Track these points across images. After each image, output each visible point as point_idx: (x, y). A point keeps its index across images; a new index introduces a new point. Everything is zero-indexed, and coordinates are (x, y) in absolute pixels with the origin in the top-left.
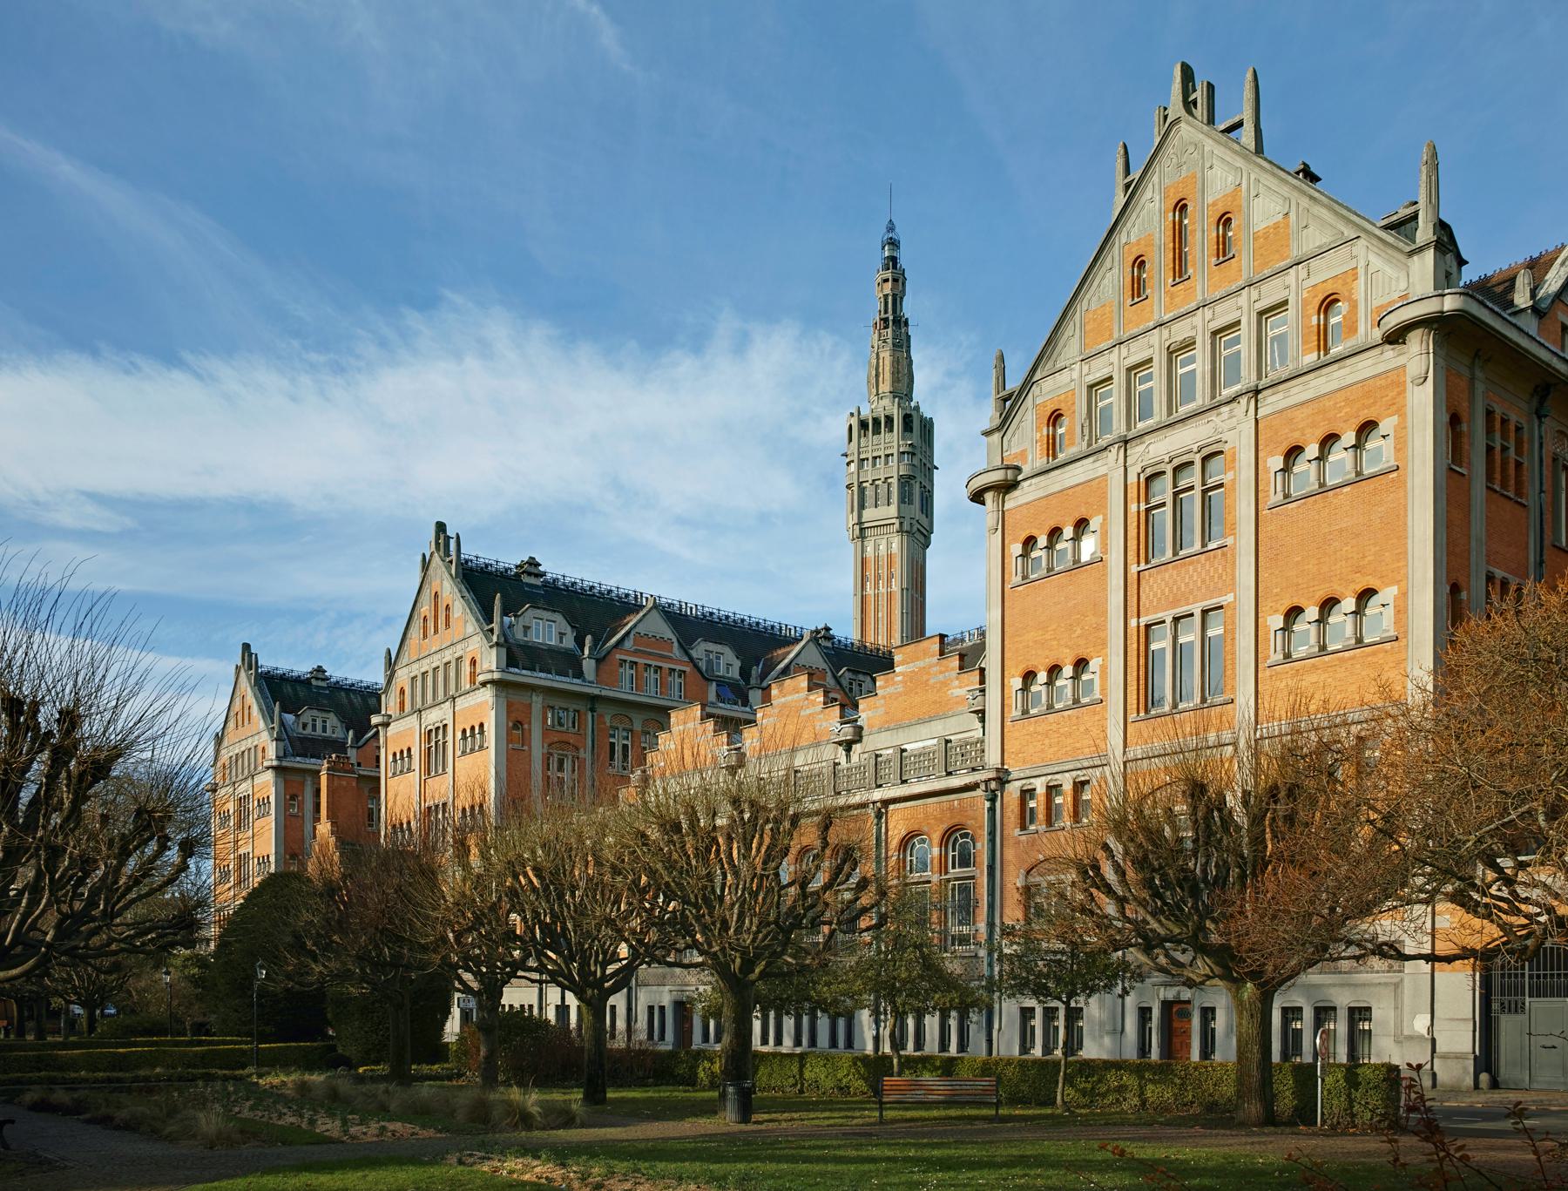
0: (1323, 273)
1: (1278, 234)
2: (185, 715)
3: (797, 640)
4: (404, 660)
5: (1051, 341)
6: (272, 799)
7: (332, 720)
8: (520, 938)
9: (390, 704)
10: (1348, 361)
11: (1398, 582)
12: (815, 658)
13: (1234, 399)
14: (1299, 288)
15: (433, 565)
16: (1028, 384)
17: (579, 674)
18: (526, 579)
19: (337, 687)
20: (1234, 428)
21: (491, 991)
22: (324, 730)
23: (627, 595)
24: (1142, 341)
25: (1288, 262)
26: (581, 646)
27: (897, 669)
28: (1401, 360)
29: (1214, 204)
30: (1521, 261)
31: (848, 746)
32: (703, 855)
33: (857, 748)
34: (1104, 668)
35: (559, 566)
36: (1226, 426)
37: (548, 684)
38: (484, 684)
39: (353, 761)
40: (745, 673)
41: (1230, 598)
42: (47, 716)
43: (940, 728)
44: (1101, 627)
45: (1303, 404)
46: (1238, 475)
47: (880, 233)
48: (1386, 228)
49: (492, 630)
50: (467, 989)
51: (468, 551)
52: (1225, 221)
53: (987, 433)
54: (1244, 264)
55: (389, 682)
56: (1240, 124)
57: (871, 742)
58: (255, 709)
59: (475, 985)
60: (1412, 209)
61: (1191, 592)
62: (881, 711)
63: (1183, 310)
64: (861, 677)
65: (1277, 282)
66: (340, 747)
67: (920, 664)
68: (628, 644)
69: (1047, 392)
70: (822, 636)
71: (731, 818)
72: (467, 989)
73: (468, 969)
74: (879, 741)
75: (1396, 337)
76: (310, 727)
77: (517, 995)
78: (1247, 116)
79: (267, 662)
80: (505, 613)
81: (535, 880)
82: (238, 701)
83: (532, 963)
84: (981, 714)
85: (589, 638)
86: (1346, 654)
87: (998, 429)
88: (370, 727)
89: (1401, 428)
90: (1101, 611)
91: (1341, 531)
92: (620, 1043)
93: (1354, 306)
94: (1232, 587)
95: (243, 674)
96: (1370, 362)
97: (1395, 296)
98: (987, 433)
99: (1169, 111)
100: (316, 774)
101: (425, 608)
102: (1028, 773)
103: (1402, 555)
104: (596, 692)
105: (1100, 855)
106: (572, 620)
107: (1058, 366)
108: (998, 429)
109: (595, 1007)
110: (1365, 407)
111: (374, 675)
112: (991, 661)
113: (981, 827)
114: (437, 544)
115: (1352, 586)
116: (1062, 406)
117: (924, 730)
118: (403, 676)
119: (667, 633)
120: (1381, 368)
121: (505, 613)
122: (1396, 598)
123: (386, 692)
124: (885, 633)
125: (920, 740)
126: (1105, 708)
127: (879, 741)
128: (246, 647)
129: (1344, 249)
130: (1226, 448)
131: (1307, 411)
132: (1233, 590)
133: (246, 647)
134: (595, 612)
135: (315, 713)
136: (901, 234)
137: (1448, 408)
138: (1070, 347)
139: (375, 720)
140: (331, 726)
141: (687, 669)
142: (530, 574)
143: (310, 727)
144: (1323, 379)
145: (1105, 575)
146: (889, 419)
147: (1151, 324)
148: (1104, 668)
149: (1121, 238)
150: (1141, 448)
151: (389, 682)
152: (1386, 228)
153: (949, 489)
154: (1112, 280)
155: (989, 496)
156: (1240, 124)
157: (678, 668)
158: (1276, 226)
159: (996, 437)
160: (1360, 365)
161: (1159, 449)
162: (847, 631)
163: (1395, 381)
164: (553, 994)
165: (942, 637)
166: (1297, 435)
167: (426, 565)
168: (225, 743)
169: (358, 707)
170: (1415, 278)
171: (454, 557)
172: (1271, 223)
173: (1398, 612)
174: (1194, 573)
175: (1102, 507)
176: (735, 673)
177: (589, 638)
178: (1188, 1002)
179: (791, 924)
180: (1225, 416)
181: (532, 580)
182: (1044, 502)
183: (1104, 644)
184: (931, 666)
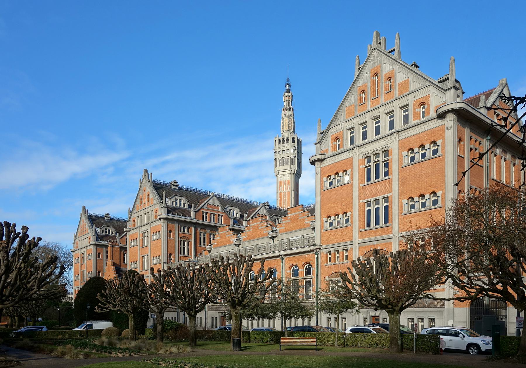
0: (420, 96)
1: (405, 85)
2: (59, 232)
3: (258, 206)
4: (135, 211)
5: (336, 116)
6: (93, 254)
7: (184, 201)
8: (169, 295)
9: (130, 224)
10: (427, 123)
11: (442, 190)
12: (263, 211)
13: (392, 134)
14: (411, 100)
15: (143, 182)
16: (329, 129)
17: (190, 216)
18: (173, 187)
19: (113, 219)
20: (393, 144)
21: (161, 312)
22: (109, 232)
23: (205, 192)
24: (363, 116)
25: (408, 93)
26: (116, 235)
27: (289, 215)
28: (351, 156)
29: (386, 75)
30: (482, 92)
31: (273, 238)
32: (225, 270)
33: (240, 246)
34: (352, 215)
35: (183, 181)
36: (390, 142)
37: (180, 219)
38: (160, 219)
39: (118, 242)
40: (242, 216)
41: (391, 194)
42: (18, 229)
43: (301, 233)
44: (351, 202)
45: (413, 136)
46: (394, 158)
47: (285, 81)
48: (439, 82)
49: (162, 202)
50: (154, 311)
51: (155, 178)
52: (390, 79)
53: (316, 144)
54: (396, 93)
55: (130, 218)
56: (394, 50)
57: (280, 237)
58: (87, 226)
59: (156, 311)
60: (447, 77)
61: (379, 192)
62: (284, 228)
63: (376, 107)
64: (278, 217)
65: (405, 99)
66: (114, 238)
67: (296, 213)
68: (205, 207)
69: (333, 132)
70: (266, 205)
71: (235, 260)
72: (154, 311)
73: (153, 305)
74: (284, 237)
75: (442, 116)
76: (174, 203)
77: (169, 315)
78: (396, 48)
79: (91, 212)
80: (166, 197)
81: (174, 278)
82: (81, 223)
83: (174, 303)
84: (314, 229)
85: (118, 234)
86: (427, 211)
87: (319, 143)
88: (124, 232)
89: (352, 172)
90: (351, 197)
91: (425, 174)
92: (202, 328)
93: (429, 106)
94: (391, 191)
95: (83, 215)
96: (434, 123)
97: (442, 103)
98: (316, 144)
99: (372, 46)
100: (106, 246)
101: (141, 195)
102: (329, 247)
103: (444, 181)
104: (195, 221)
105: (347, 271)
106: (188, 199)
107: (338, 124)
108: (319, 143)
109: (193, 317)
110: (432, 137)
111: (125, 216)
112: (318, 213)
113: (314, 263)
114: (145, 176)
115: (428, 191)
116: (339, 136)
117: (297, 234)
118: (134, 216)
119: (218, 203)
120: (437, 125)
121: (166, 197)
122: (442, 195)
123: (129, 221)
124: (288, 203)
125: (296, 236)
126: (352, 227)
127: (284, 237)
128: (84, 207)
129: (426, 89)
130: (389, 149)
131: (414, 138)
132: (392, 192)
133: (84, 207)
134: (196, 197)
135: (106, 227)
136: (291, 82)
137: (458, 137)
138: (342, 117)
139: (125, 230)
140: (112, 231)
141: (224, 215)
142: (174, 185)
143: (174, 203)
144: (419, 128)
145: (352, 187)
146: (288, 140)
147: (366, 111)
148: (352, 215)
149: (356, 85)
150: (363, 149)
151: (130, 218)
152: (439, 82)
153: (305, 161)
154: (354, 98)
155: (316, 163)
156: (394, 50)
157: (221, 214)
158: (405, 81)
159: (318, 145)
160: (431, 124)
161: (370, 149)
162: (275, 203)
163: (442, 130)
164: (181, 314)
165: (303, 205)
166: (411, 145)
167: (141, 182)
168: (78, 237)
169: (120, 226)
170: (448, 98)
171: (150, 180)
172: (403, 80)
173: (442, 199)
174: (379, 187)
175: (351, 166)
176: (238, 216)
177: (118, 234)
178: (378, 316)
179: (241, 292)
180: (389, 139)
181: (175, 187)
182: (333, 165)
183: (352, 208)
184: (299, 214)
